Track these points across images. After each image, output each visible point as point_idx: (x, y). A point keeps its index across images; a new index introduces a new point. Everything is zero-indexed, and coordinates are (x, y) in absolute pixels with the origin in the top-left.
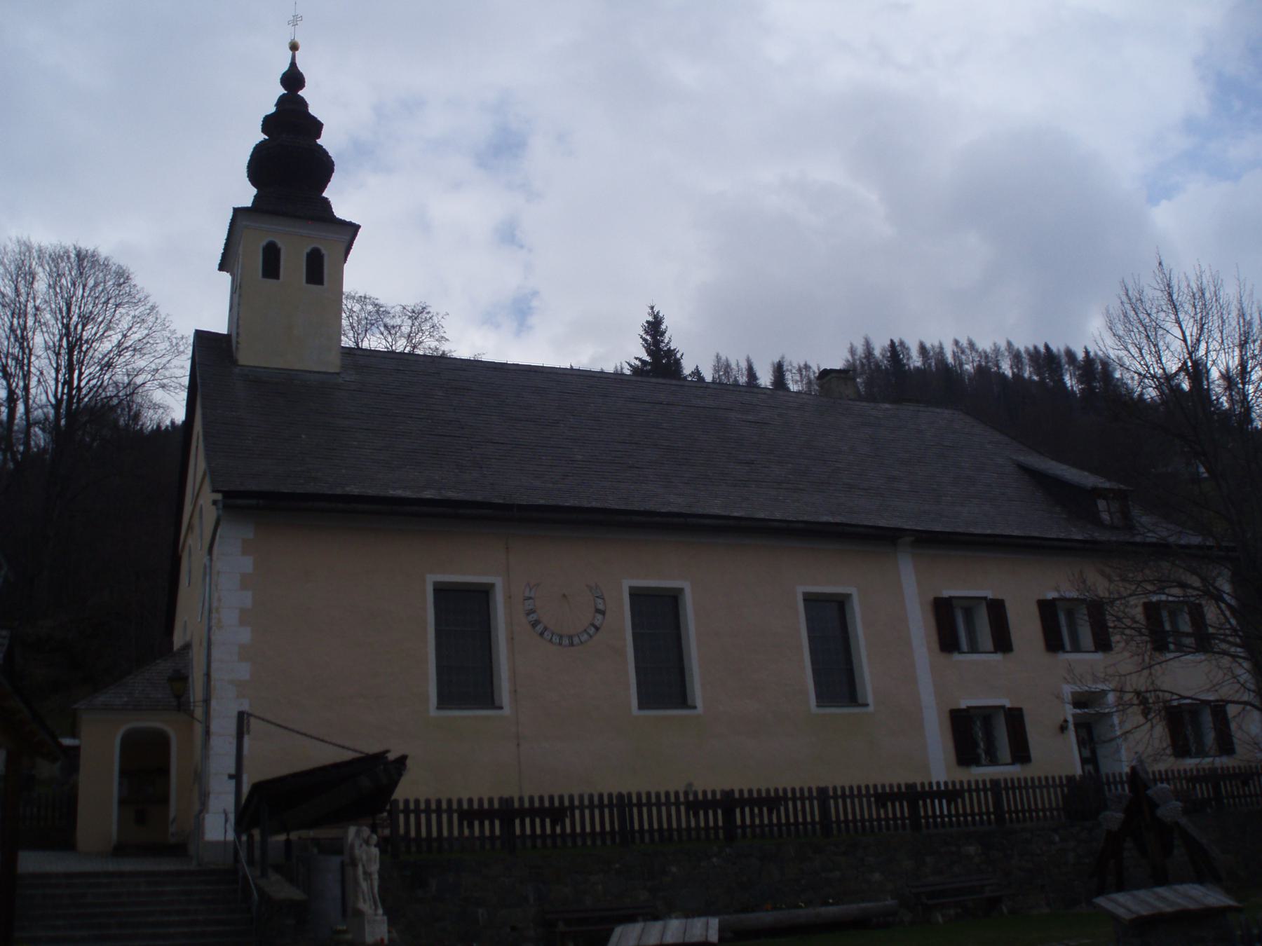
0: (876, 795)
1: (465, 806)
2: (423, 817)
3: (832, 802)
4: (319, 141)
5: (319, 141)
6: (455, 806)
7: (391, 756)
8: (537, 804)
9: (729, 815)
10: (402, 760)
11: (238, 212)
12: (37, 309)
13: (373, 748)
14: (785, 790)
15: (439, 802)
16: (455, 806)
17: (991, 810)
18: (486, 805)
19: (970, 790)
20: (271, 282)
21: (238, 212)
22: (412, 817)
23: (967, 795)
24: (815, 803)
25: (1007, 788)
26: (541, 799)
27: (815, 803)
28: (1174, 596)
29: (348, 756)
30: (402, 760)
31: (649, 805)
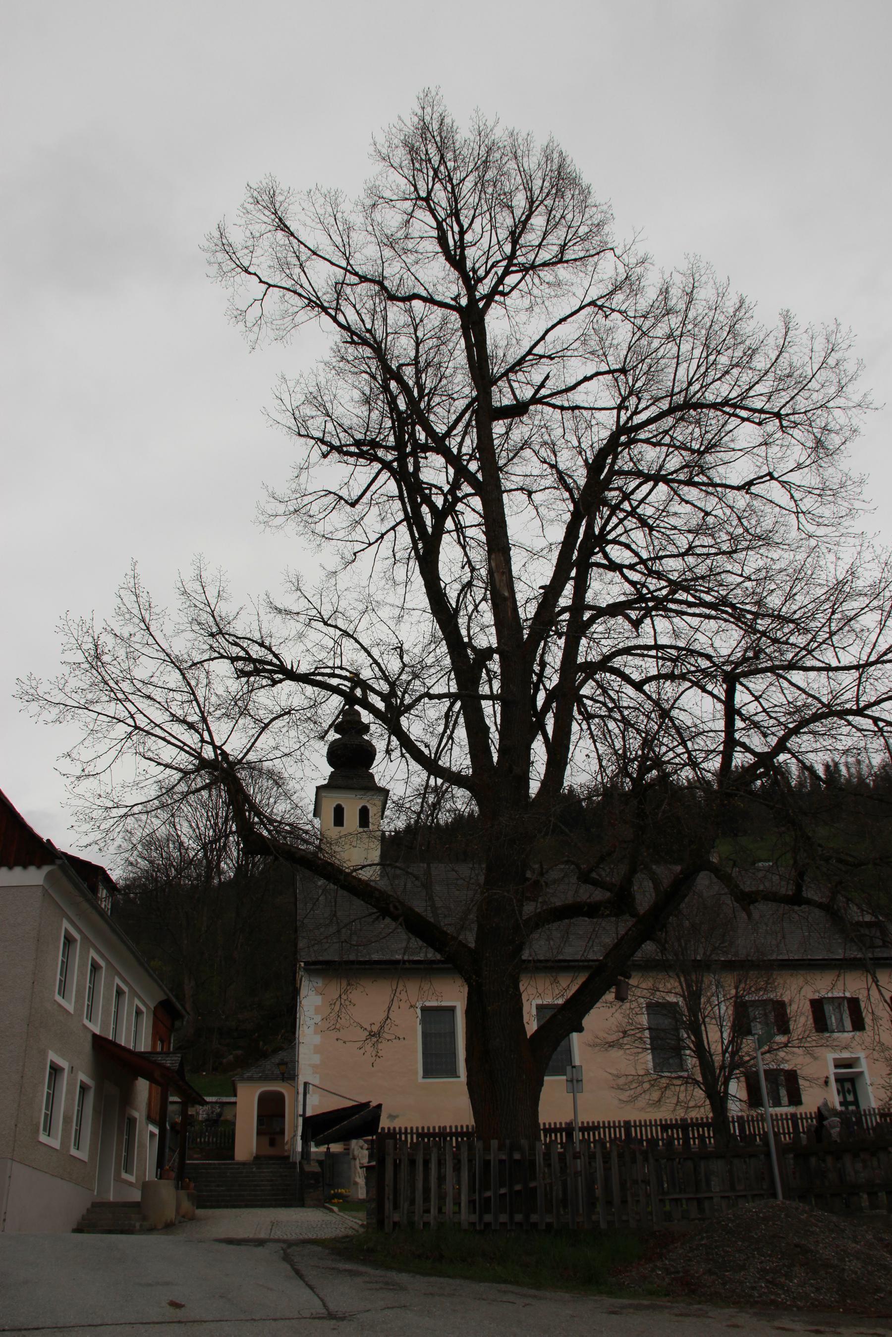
0: (661, 1125)
1: (420, 1131)
2: (638, 1129)
3: (633, 1129)
4: (333, 770)
5: (333, 770)
6: (415, 1131)
7: (374, 1104)
8: (459, 1130)
9: (570, 1135)
10: (379, 1106)
11: (319, 789)
12: (861, 545)
13: (363, 1100)
14: (598, 1122)
15: (406, 1129)
16: (415, 1131)
17: (791, 1130)
18: (431, 1131)
19: (604, 1127)
20: (339, 828)
21: (319, 789)
22: (612, 1130)
23: (602, 1130)
24: (623, 1129)
25: (802, 1119)
26: (456, 1127)
27: (623, 1129)
28: (841, 1019)
29: (351, 1104)
30: (379, 1106)
31: (609, 1127)
